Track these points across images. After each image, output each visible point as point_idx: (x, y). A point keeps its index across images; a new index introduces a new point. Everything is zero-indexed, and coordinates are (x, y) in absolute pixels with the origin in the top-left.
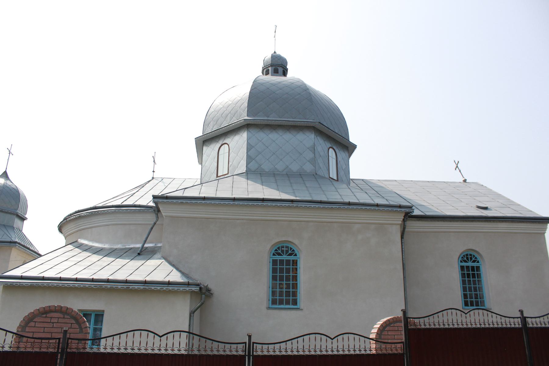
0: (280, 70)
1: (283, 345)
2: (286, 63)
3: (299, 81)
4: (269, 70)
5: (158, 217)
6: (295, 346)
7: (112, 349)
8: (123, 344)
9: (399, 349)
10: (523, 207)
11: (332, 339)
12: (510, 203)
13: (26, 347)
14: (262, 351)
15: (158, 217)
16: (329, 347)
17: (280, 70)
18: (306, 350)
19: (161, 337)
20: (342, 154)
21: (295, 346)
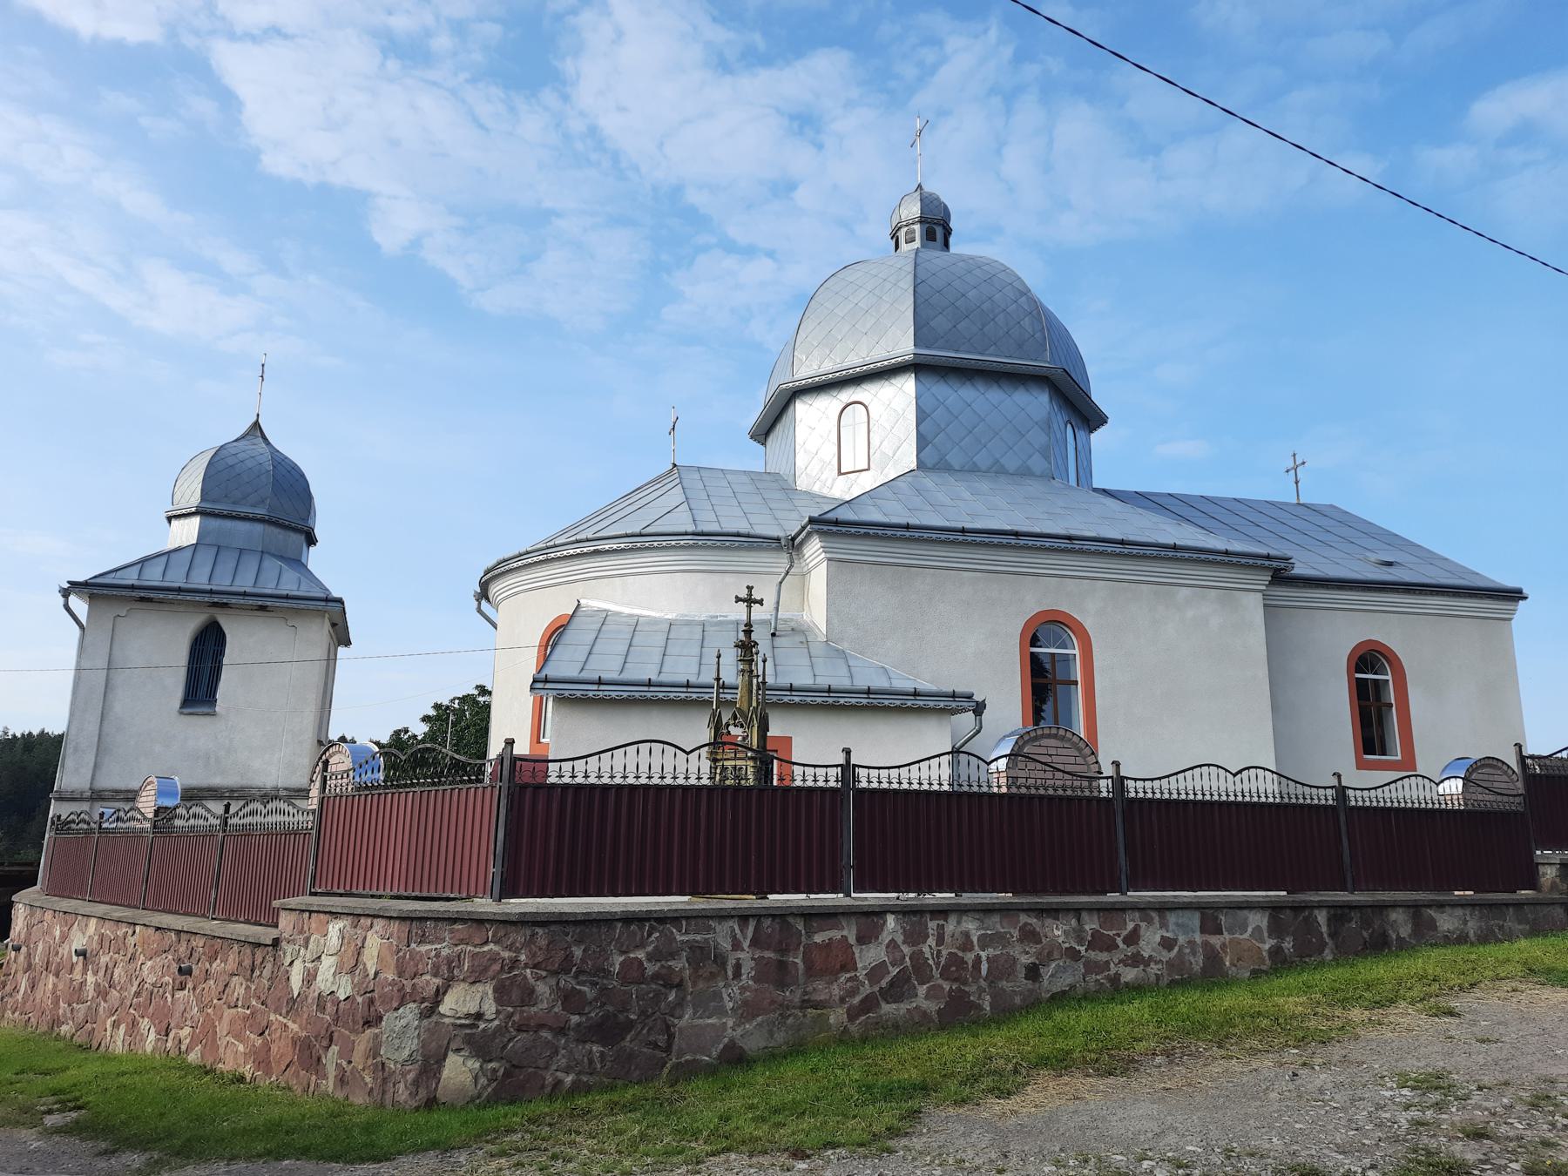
0: (939, 231)
1: (580, 765)
2: (938, 199)
3: (1005, 269)
4: (913, 231)
5: (792, 561)
6: (606, 768)
7: (625, 777)
8: (619, 768)
9: (1516, 804)
10: (1457, 565)
11: (688, 753)
12: (1430, 557)
13: (1486, 800)
14: (804, 780)
15: (792, 561)
16: (681, 769)
17: (939, 231)
18: (631, 776)
19: (688, 753)
20: (1081, 434)
21: (924, 775)
